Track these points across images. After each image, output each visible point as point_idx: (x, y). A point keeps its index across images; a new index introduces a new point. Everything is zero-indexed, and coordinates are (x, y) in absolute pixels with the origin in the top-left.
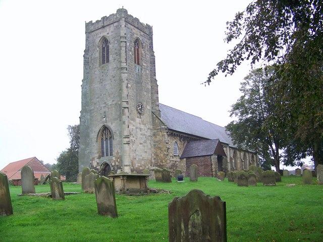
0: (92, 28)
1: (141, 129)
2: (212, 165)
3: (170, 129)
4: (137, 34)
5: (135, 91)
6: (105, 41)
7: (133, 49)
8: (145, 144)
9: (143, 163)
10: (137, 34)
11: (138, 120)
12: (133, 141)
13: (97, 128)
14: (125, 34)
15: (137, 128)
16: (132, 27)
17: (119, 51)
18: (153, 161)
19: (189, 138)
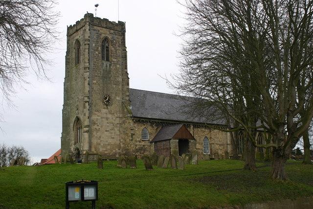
0: (71, 32)
1: (107, 119)
2: (170, 148)
3: (135, 117)
4: (105, 33)
5: (101, 85)
6: (78, 41)
7: (100, 48)
8: (112, 131)
9: (109, 147)
10: (105, 33)
11: (104, 111)
12: (98, 129)
13: (73, 119)
14: (89, 37)
15: (102, 118)
16: (99, 28)
17: (99, 45)
18: (122, 146)
19: (162, 123)
